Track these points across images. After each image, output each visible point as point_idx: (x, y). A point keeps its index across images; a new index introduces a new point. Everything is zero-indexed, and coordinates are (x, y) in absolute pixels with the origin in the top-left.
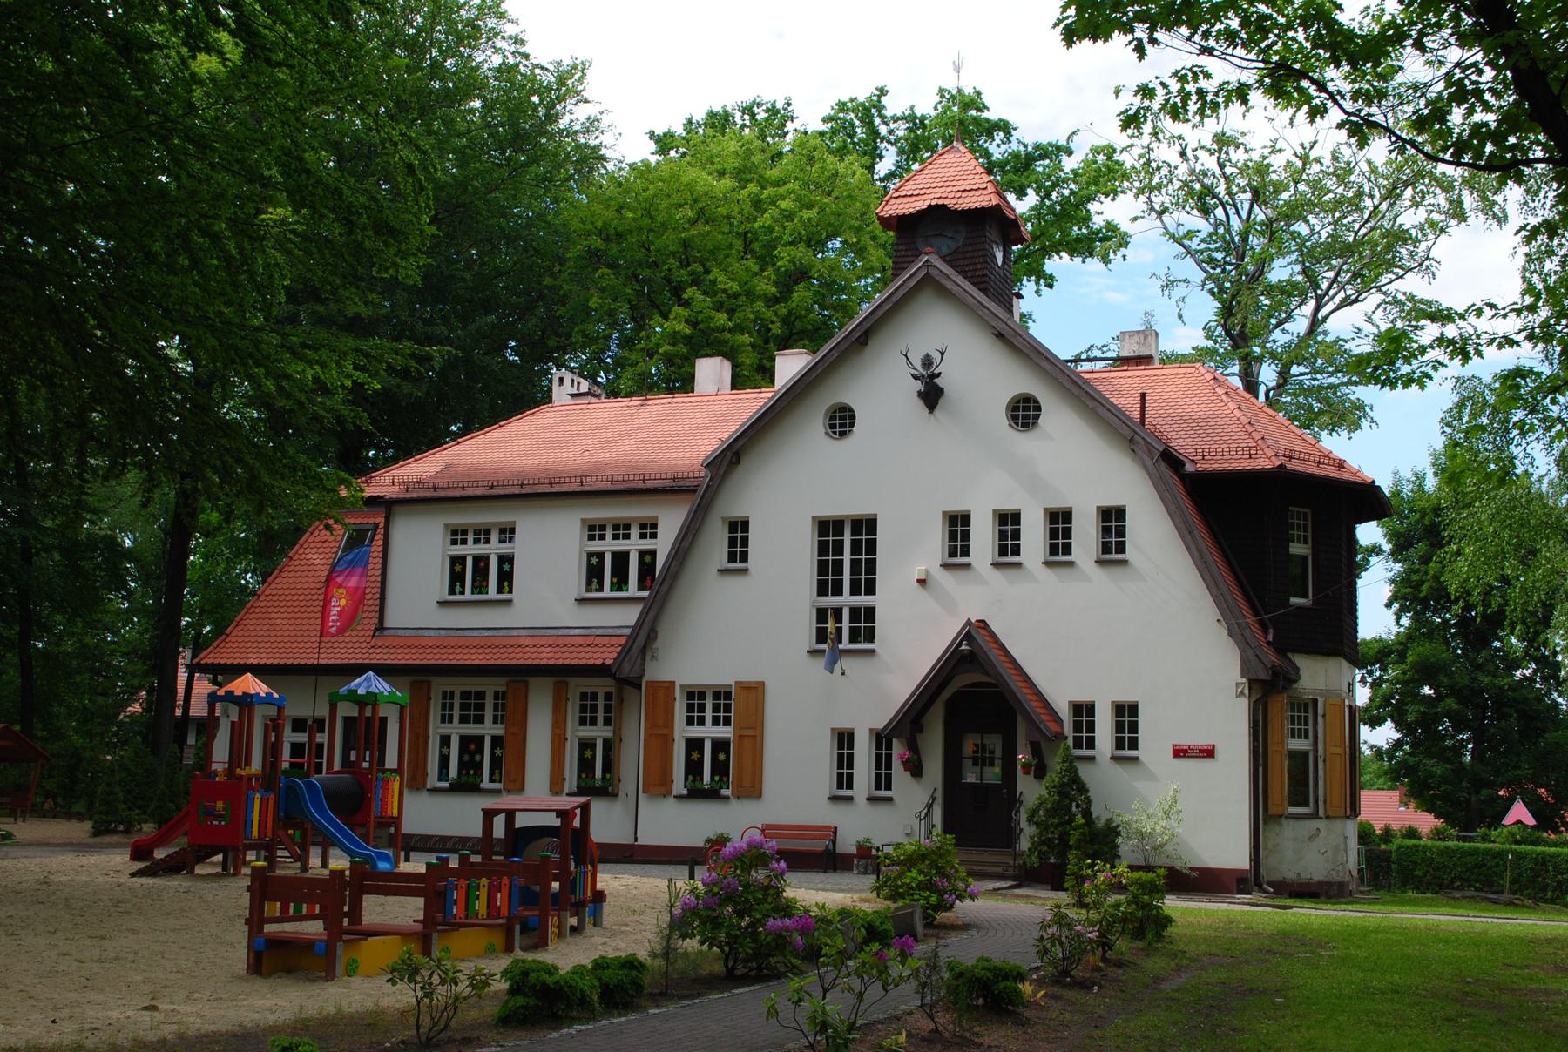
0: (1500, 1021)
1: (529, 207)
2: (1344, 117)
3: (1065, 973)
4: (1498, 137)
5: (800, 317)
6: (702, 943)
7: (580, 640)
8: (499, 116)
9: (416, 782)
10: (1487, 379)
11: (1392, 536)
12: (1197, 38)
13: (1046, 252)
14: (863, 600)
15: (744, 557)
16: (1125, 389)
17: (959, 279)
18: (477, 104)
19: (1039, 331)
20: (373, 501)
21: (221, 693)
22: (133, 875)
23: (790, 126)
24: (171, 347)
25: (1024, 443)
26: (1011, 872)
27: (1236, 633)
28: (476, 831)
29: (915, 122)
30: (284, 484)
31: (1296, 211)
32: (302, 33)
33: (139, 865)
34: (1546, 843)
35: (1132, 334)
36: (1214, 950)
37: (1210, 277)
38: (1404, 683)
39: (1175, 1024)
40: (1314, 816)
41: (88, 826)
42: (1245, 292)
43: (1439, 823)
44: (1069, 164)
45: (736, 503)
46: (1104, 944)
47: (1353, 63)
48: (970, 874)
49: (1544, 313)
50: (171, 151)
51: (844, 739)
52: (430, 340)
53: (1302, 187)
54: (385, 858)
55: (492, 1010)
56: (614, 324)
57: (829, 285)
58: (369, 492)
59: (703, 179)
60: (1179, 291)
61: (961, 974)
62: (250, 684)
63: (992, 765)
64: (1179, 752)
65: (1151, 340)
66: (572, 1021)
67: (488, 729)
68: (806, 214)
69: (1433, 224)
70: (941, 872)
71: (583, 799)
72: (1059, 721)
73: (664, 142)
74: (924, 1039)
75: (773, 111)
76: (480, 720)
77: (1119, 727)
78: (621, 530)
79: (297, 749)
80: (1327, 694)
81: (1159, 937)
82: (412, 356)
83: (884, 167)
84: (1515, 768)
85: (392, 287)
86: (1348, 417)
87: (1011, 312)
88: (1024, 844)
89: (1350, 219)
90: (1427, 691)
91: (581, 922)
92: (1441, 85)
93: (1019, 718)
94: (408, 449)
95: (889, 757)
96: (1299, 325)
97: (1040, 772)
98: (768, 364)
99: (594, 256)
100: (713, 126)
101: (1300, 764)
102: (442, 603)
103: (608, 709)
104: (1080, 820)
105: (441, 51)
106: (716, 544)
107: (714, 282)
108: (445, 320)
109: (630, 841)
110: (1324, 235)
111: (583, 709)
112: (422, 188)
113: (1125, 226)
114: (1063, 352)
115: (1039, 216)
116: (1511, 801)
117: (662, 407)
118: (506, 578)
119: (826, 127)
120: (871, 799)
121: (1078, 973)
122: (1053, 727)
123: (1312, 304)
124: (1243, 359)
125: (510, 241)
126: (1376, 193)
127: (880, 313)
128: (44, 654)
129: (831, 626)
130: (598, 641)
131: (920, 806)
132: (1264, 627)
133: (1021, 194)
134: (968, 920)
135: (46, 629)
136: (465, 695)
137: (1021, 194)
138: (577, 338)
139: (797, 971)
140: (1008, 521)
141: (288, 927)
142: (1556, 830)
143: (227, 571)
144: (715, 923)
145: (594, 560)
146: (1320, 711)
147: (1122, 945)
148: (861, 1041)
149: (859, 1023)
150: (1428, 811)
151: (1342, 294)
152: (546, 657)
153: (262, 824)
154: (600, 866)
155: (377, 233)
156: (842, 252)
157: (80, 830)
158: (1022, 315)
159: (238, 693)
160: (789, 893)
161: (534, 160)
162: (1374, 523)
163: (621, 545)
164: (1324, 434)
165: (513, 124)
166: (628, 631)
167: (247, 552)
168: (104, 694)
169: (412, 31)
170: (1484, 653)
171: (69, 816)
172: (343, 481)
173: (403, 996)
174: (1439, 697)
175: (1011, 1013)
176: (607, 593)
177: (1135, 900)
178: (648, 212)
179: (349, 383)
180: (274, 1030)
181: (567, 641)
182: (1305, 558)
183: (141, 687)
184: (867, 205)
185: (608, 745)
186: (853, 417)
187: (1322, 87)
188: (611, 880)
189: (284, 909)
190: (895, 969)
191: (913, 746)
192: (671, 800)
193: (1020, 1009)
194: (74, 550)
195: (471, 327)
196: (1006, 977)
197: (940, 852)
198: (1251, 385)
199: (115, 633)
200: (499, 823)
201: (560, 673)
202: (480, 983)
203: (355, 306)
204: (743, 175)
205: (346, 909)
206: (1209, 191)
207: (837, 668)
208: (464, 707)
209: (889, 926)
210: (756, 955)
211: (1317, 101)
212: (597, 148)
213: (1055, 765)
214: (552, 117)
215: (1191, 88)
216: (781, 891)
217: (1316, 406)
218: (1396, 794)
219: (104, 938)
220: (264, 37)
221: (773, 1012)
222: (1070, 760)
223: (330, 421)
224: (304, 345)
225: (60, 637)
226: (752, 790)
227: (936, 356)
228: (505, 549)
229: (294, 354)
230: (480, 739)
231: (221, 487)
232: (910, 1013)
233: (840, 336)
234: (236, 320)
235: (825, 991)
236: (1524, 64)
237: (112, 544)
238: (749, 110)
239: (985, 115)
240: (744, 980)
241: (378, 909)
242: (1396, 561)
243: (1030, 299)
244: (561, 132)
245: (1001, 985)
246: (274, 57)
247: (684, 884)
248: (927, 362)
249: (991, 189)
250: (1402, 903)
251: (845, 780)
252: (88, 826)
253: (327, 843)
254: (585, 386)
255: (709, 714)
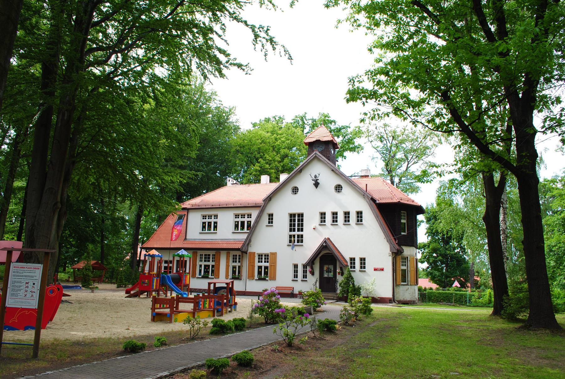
0: (449, 333)
1: (222, 140)
2: (411, 120)
3: (347, 322)
4: (447, 125)
5: (286, 166)
6: (260, 315)
7: (233, 242)
8: (216, 118)
9: (194, 276)
10: (447, 181)
11: (427, 218)
12: (377, 101)
13: (344, 151)
14: (300, 233)
15: (272, 223)
16: (362, 183)
17: (323, 157)
18: (210, 116)
19: (342, 170)
20: (184, 209)
21: (147, 254)
22: (126, 297)
23: (284, 121)
24: (137, 172)
25: (338, 195)
26: (335, 298)
27: (389, 241)
28: (207, 288)
29: (314, 121)
30: (163, 205)
31: (402, 142)
32: (169, 99)
33: (127, 295)
34: (463, 291)
35: (364, 170)
36: (383, 317)
37: (383, 157)
38: (429, 253)
39: (372, 335)
40: (408, 285)
41: (116, 285)
42: (391, 160)
43: (438, 286)
44: (349, 130)
45: (269, 210)
46: (356, 315)
47: (413, 107)
48: (325, 299)
49: (459, 165)
50: (138, 126)
51: (296, 266)
52: (198, 171)
53: (404, 136)
54: (185, 294)
55: (209, 331)
56: (242, 167)
57: (293, 158)
58: (183, 206)
59: (264, 133)
60: (376, 160)
61: (321, 323)
62: (154, 252)
63: (331, 272)
64: (375, 270)
65: (369, 171)
66: (228, 333)
67: (211, 263)
68: (287, 142)
69: (434, 145)
70: (318, 298)
71: (232, 280)
72: (347, 262)
73: (254, 125)
74: (312, 338)
75: (280, 118)
76: (209, 261)
77: (361, 264)
78: (243, 216)
79: (165, 268)
80: (410, 256)
81: (370, 314)
82: (194, 174)
83: (306, 131)
84: (455, 273)
85: (189, 158)
86: (415, 190)
87: (335, 165)
88: (338, 292)
89: (415, 143)
90: (435, 255)
91: (231, 310)
92: (434, 113)
93: (337, 262)
94: (193, 197)
95: (306, 270)
96: (404, 168)
97: (342, 274)
98: (278, 177)
99: (238, 151)
100: (266, 121)
101: (404, 272)
102: (200, 233)
103: (239, 259)
104: (351, 286)
105: (202, 103)
106: (265, 219)
107: (266, 157)
108: (202, 166)
109: (244, 290)
110: (409, 147)
111: (233, 259)
112: (196, 135)
113: (363, 145)
114: (348, 174)
115: (343, 142)
116: (454, 281)
117: (253, 187)
118: (215, 227)
119: (293, 121)
120: (302, 281)
121: (350, 322)
122: (345, 263)
123: (406, 163)
124: (391, 176)
125: (218, 147)
126: (421, 137)
127: (305, 165)
128: (107, 244)
129: (293, 239)
130: (237, 242)
131: (314, 282)
132: (395, 240)
133: (338, 137)
134: (324, 310)
135: (107, 238)
136: (205, 255)
137: (338, 137)
138: (233, 170)
139: (282, 322)
140: (335, 214)
141: (162, 310)
142: (465, 288)
143: (150, 225)
144: (263, 310)
145: (236, 223)
146: (409, 260)
147: (361, 316)
148: (297, 339)
149: (296, 335)
150: (435, 283)
151: (414, 161)
152: (225, 246)
153: (156, 286)
154: (236, 296)
155: (185, 146)
156: (296, 151)
157: (114, 286)
158: (338, 166)
159: (151, 254)
160: (281, 303)
161: (224, 129)
162: (422, 215)
163: (210, 220)
164: (410, 194)
165: (219, 120)
166: (244, 240)
167: (155, 221)
168: (121, 254)
169: (196, 99)
170: (448, 246)
171: (112, 283)
172: (177, 204)
173: (187, 327)
174: (438, 256)
175: (333, 332)
176: (239, 231)
177: (364, 305)
178: (250, 141)
179: (178, 181)
180: (157, 335)
181: (230, 242)
182: (405, 223)
183: (129, 252)
184: (302, 140)
185: (239, 267)
186: (298, 189)
187: (406, 113)
188: (238, 299)
189: (160, 306)
190: (305, 321)
191: (312, 268)
192: (254, 281)
193: (335, 331)
194: (114, 220)
195: (208, 168)
196: (332, 323)
197: (317, 293)
198: (393, 183)
199: (123, 239)
200: (212, 286)
201: (228, 250)
202: (205, 324)
203: (181, 163)
204: (273, 133)
205: (175, 306)
206: (382, 137)
207: (294, 249)
208: (205, 258)
209: (305, 311)
210: (272, 318)
211: (405, 116)
212: (238, 126)
213: (346, 272)
214: (228, 119)
215: (376, 113)
216: (278, 303)
217: (408, 187)
218: (428, 279)
219: (118, 312)
220: (160, 100)
221: (275, 332)
222: (349, 271)
223: (174, 190)
224: (168, 172)
225: (111, 240)
226: (274, 278)
227: (318, 175)
228: (215, 220)
229: (165, 174)
230: (209, 266)
231: (148, 205)
232: (309, 332)
233: (295, 170)
234: (152, 166)
235: (288, 327)
236: (452, 108)
237: (123, 218)
238: (274, 118)
239: (329, 119)
240: (270, 324)
241: (183, 306)
242: (427, 224)
243: (340, 161)
244: (230, 122)
245: (331, 325)
246: (162, 105)
247: (255, 300)
248: (316, 177)
249: (331, 136)
250: (428, 305)
251: (296, 276)
252: (116, 285)
253: (172, 290)
254: (235, 182)
255: (263, 260)
